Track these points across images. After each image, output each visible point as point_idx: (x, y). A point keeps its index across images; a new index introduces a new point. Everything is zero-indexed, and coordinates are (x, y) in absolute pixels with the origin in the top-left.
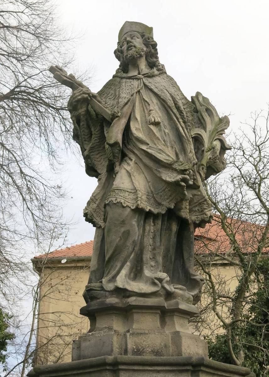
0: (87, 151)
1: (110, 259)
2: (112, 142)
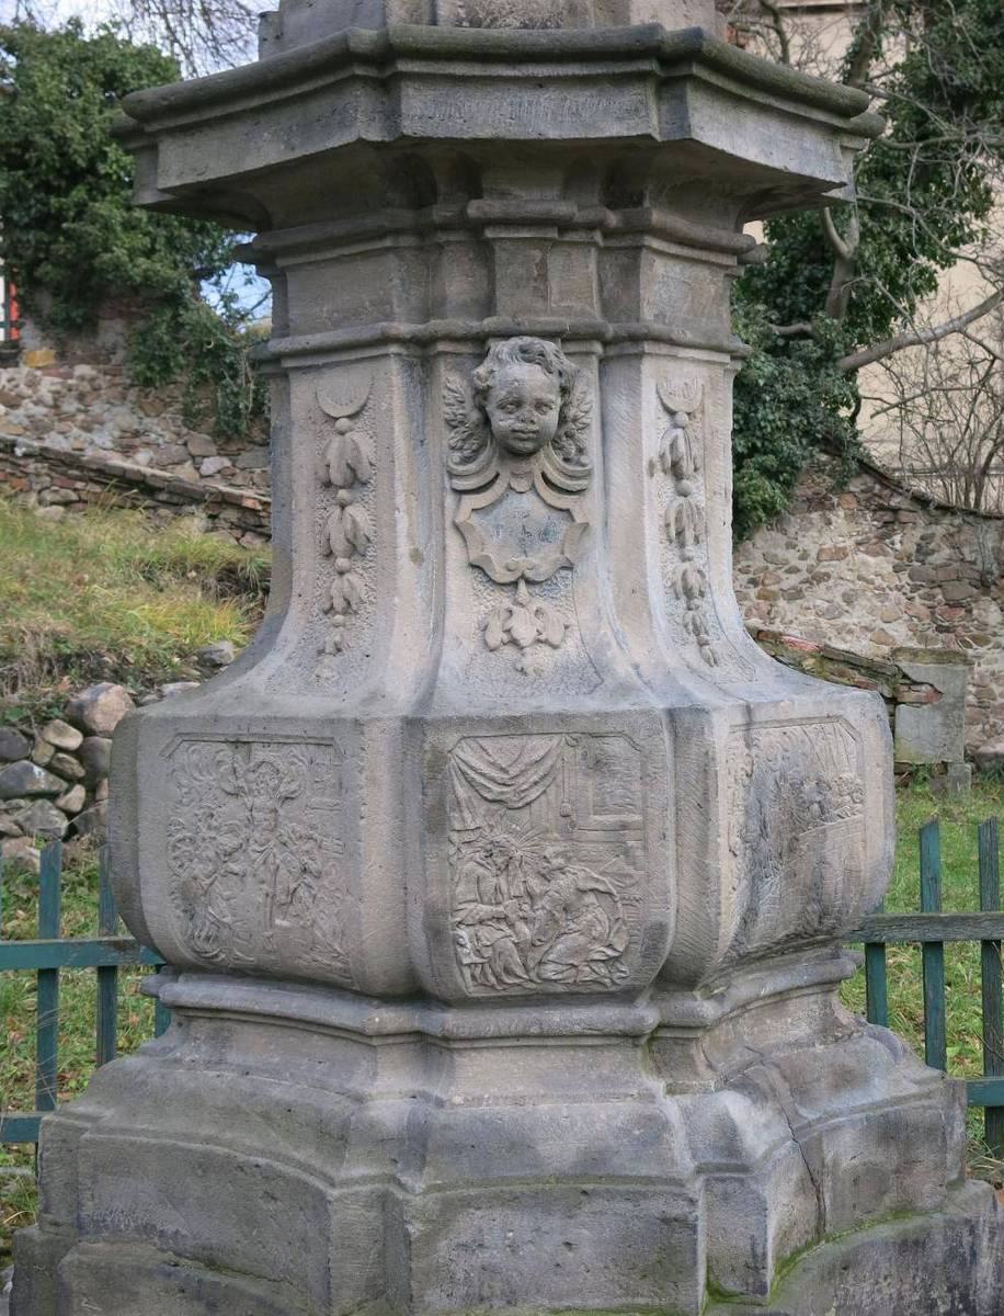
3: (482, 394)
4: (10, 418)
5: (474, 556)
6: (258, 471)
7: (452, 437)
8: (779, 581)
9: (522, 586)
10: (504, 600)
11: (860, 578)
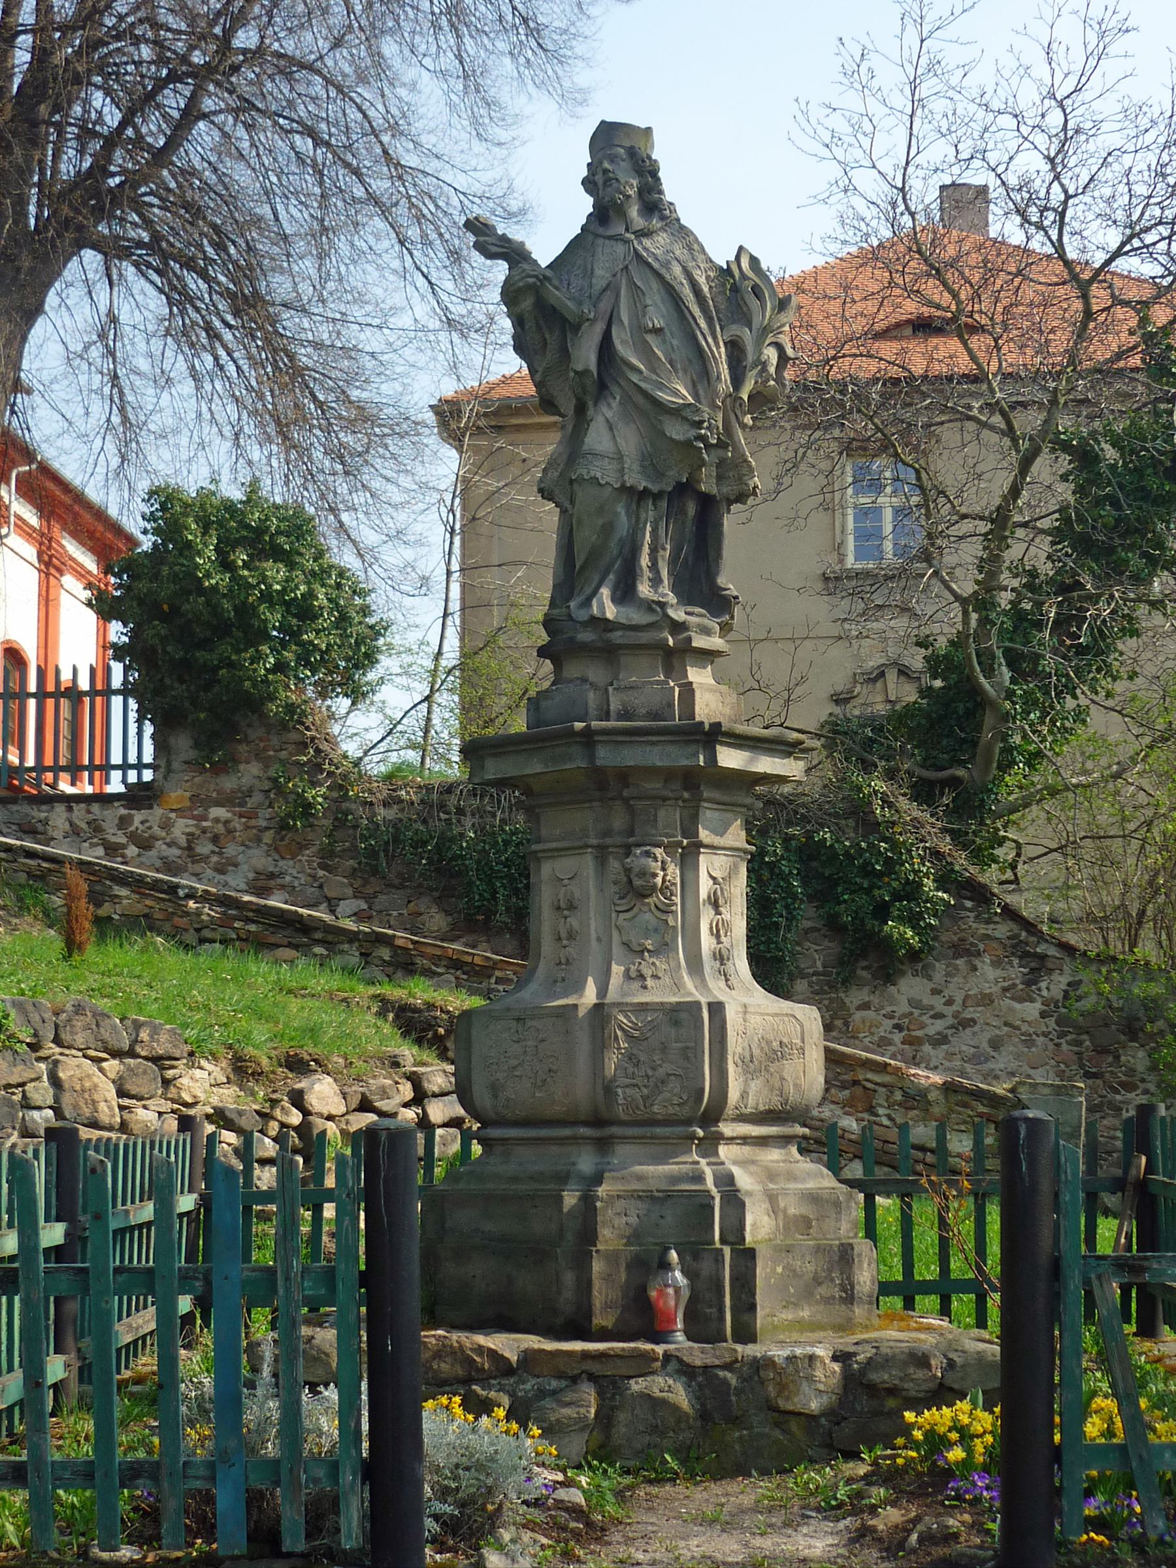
1: (582, 568)
2: (580, 368)
4: (143, 859)
5: (625, 939)
6: (395, 913)
7: (614, 888)
8: (922, 1026)
11: (1006, 1024)
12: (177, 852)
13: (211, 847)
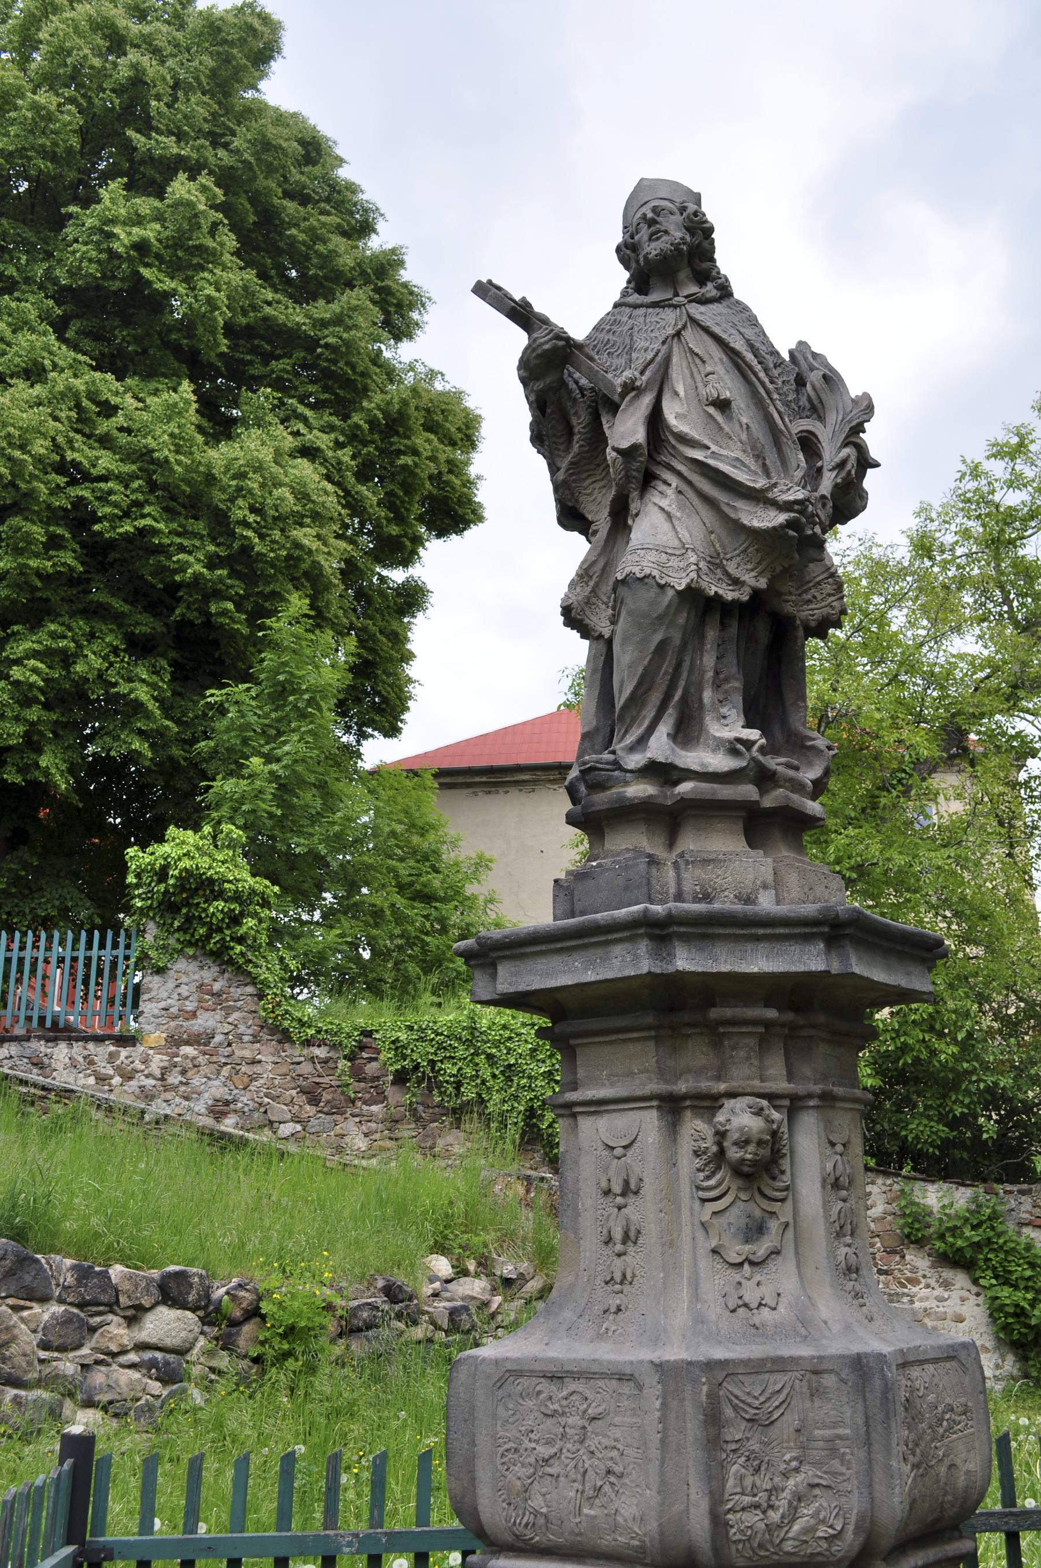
0: (562, 470)
3: (721, 1135)
7: (698, 1163)
9: (746, 1266)
10: (735, 1276)
12: (153, 1082)
13: (180, 1078)
